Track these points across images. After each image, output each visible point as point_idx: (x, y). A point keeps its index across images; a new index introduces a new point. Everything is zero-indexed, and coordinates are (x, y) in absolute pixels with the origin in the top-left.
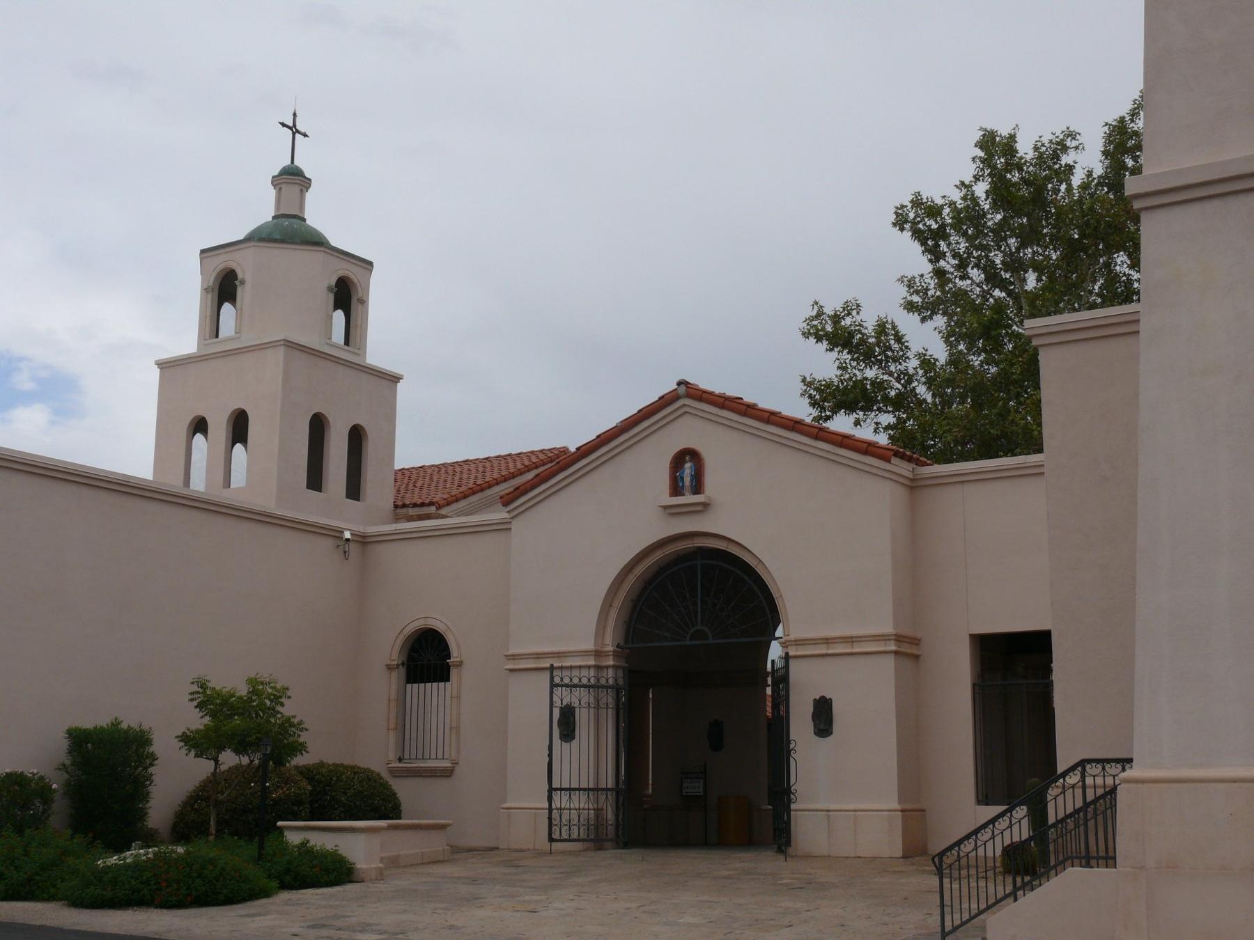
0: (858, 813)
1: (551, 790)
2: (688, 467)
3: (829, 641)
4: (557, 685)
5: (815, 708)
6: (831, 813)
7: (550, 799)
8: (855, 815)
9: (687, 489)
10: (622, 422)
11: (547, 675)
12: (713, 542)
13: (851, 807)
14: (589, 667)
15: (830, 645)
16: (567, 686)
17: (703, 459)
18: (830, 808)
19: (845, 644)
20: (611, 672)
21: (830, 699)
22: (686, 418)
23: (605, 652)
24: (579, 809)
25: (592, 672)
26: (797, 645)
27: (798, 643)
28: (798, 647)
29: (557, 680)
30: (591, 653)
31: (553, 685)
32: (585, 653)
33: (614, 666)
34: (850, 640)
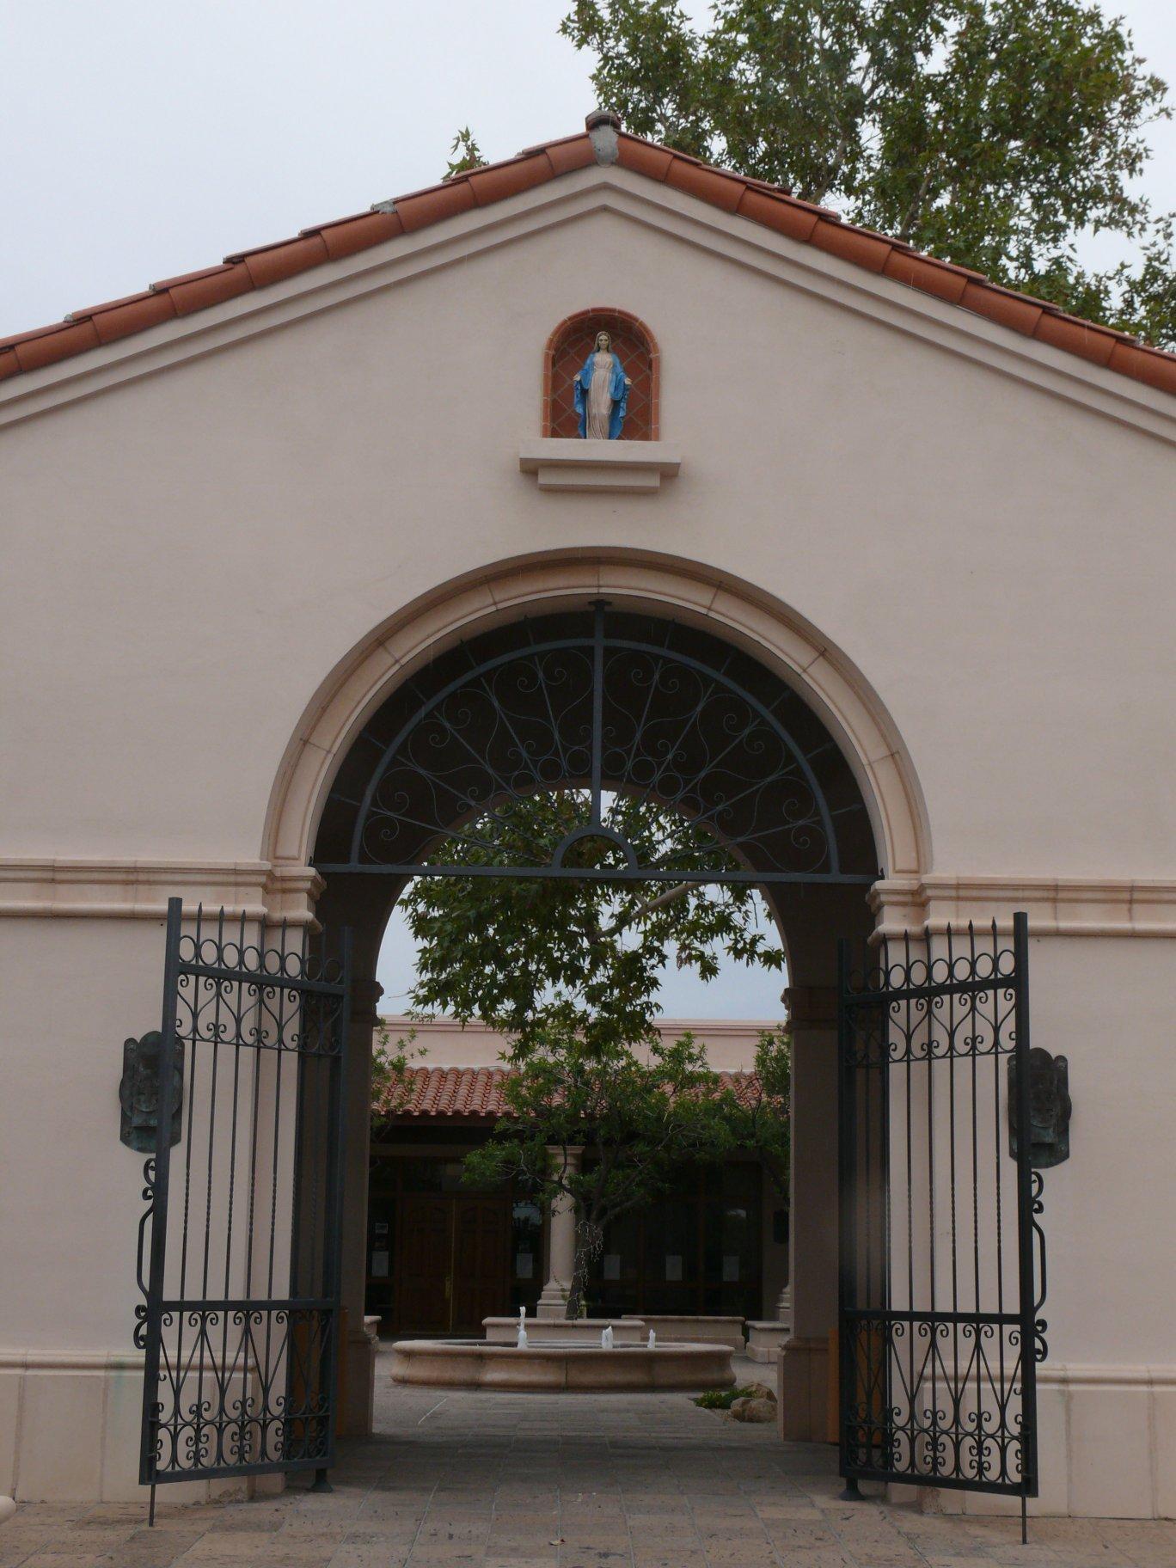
0: (1157, 1389)
1: (154, 1311)
2: (603, 370)
3: (1137, 896)
4: (186, 969)
5: (128, 1067)
6: (1073, 1388)
7: (151, 1342)
8: (1062, 1393)
9: (597, 425)
10: (396, 202)
11: (160, 935)
12: (633, 583)
13: (1140, 1370)
14: (243, 919)
15: (1061, 906)
16: (963, 987)
17: (655, 345)
18: (1070, 1374)
19: (1108, 906)
20: (295, 942)
21: (1062, 1059)
22: (604, 224)
23: (284, 879)
24: (178, 1367)
25: (252, 936)
26: (958, 899)
27: (963, 893)
28: (962, 904)
29: (186, 951)
30: (253, 879)
31: (176, 969)
32: (233, 877)
33: (307, 927)
34: (1129, 896)
